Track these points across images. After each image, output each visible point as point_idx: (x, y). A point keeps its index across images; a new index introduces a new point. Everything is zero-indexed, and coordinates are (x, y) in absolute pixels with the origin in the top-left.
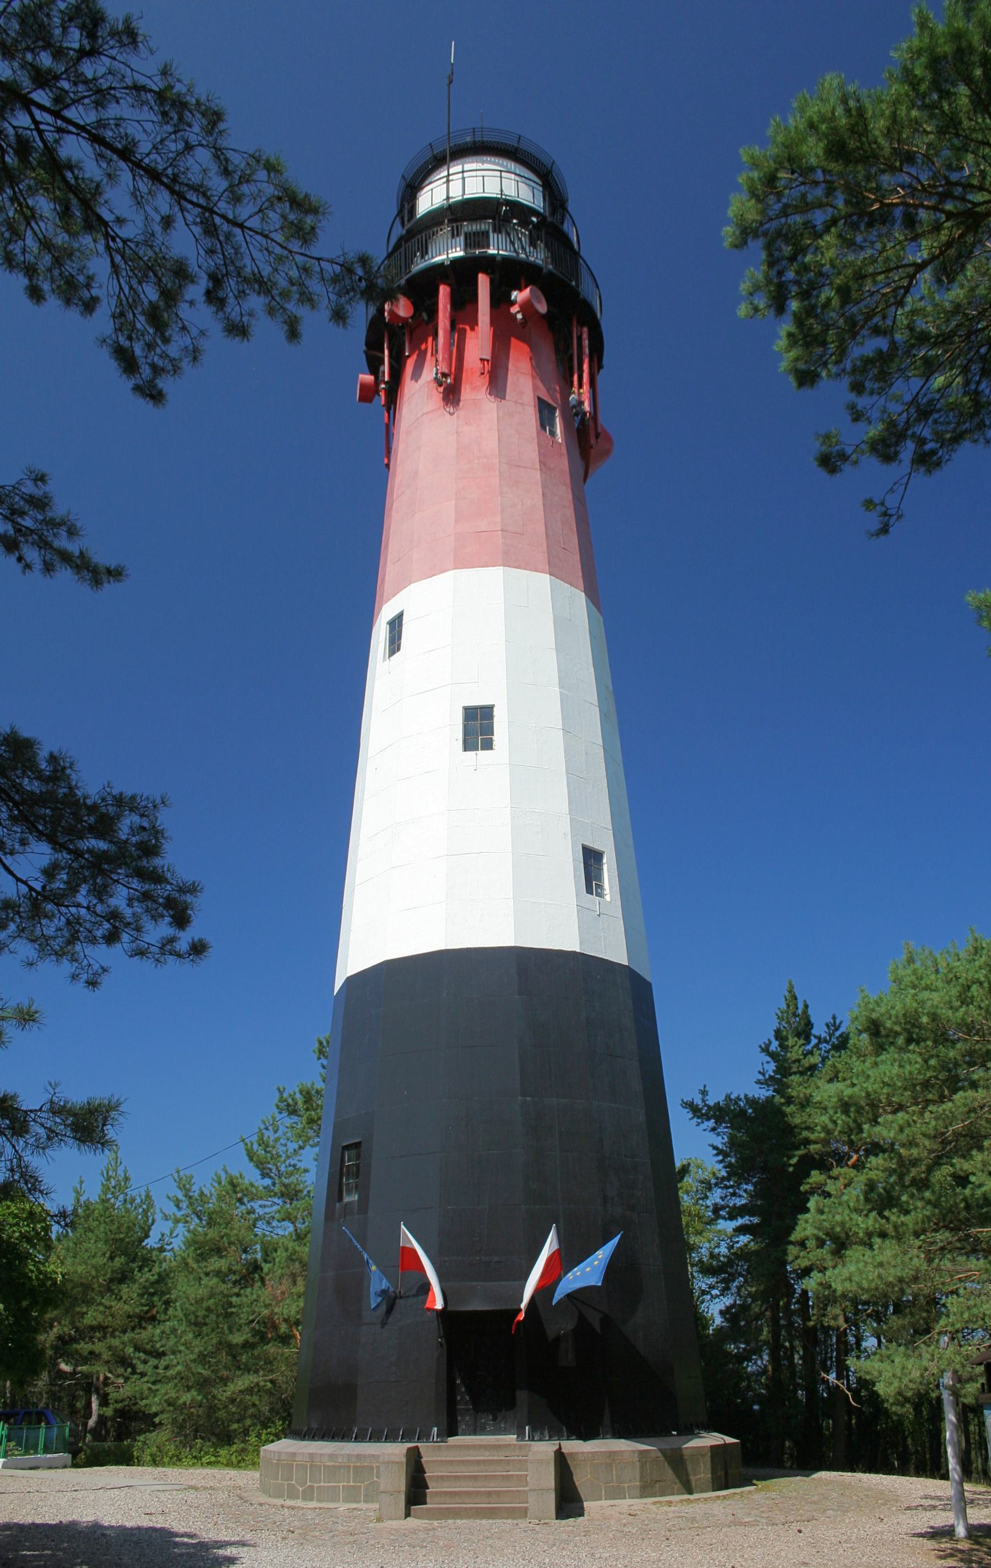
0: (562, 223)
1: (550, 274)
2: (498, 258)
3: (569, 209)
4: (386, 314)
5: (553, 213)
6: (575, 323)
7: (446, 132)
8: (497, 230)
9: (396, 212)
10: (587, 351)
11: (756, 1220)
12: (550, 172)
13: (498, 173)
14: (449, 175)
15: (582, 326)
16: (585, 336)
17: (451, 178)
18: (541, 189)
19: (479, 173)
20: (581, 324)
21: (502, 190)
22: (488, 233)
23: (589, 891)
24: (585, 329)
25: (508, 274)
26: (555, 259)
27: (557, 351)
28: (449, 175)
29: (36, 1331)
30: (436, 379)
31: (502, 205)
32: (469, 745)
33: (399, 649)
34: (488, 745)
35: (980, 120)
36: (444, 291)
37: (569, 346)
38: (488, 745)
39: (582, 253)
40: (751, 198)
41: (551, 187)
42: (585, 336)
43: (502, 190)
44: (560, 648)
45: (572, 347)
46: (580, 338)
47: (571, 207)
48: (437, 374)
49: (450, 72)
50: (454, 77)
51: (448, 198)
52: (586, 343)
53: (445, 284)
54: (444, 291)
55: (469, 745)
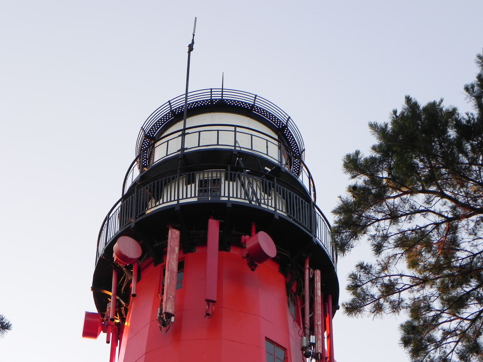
0: (298, 174)
1: (281, 218)
2: (229, 205)
4: (114, 255)
5: (290, 163)
6: (308, 266)
8: (230, 178)
11: (312, 346)
12: (286, 126)
13: (233, 128)
14: (185, 129)
15: (314, 269)
17: (187, 131)
18: (277, 143)
20: (314, 267)
21: (236, 142)
22: (219, 180)
24: (318, 272)
25: (241, 220)
26: (289, 208)
27: (289, 291)
28: (185, 129)
29: (380, 146)
30: (161, 318)
31: (236, 156)
36: (174, 236)
37: (301, 288)
39: (317, 204)
40: (366, 233)
41: (287, 140)
43: (236, 142)
45: (304, 290)
46: (312, 281)
47: (307, 159)
48: (161, 314)
50: (194, 46)
51: (183, 149)
53: (174, 228)
54: (174, 236)
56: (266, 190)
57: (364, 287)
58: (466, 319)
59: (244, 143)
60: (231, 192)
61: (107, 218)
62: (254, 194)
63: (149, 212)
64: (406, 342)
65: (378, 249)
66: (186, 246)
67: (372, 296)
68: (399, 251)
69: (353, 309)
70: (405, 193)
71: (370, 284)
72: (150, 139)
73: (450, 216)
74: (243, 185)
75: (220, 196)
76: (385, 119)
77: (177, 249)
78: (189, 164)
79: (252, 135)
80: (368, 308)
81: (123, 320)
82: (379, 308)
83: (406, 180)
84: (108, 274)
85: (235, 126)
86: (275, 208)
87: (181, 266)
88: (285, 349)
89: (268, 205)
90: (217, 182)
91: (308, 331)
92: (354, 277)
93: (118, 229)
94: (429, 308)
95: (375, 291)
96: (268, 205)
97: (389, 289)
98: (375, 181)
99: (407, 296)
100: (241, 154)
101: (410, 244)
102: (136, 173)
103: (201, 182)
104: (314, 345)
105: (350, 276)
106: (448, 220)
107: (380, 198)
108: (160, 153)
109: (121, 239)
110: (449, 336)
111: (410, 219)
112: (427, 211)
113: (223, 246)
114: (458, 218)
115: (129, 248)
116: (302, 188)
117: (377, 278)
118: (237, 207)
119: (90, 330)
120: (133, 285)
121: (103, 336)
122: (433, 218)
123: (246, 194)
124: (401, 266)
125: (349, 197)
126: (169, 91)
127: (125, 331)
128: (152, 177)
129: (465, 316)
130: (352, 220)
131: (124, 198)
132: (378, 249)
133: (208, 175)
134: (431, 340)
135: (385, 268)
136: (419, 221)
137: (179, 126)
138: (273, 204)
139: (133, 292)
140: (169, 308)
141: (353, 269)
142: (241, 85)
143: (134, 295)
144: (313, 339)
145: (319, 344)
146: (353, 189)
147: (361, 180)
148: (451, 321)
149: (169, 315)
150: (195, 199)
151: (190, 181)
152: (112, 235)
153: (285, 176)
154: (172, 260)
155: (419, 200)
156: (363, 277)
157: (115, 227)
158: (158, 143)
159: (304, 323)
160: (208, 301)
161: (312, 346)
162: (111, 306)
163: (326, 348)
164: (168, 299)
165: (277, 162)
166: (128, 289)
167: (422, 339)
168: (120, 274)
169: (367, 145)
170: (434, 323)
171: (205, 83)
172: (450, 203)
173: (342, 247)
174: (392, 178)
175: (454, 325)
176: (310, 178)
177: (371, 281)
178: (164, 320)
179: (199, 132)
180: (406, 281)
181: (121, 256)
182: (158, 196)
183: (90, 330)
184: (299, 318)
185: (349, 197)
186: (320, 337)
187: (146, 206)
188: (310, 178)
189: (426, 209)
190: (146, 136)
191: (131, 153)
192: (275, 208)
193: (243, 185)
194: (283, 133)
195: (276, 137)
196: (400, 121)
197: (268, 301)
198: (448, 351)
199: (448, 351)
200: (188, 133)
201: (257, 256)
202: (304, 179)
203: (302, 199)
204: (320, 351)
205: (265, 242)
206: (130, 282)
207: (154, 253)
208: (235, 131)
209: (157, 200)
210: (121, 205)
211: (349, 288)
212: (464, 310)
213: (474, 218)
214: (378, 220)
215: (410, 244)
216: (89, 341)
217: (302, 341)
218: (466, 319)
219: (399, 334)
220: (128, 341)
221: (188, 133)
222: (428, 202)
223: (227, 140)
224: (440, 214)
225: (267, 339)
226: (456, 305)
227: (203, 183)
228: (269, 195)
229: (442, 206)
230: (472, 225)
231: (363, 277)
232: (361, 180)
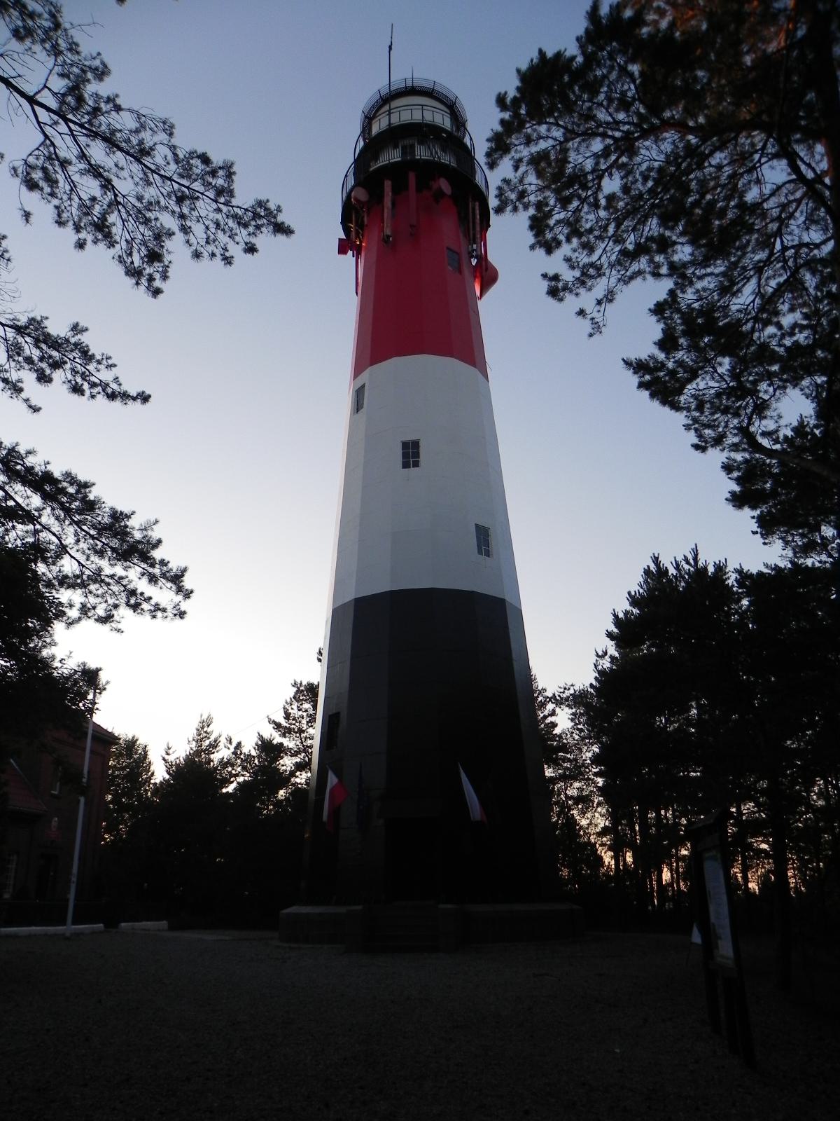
3: (468, 129)
5: (458, 129)
6: (471, 200)
7: (388, 83)
8: (421, 143)
9: (359, 133)
10: (478, 217)
11: (325, 818)
13: (421, 107)
14: (390, 110)
16: (477, 208)
17: (391, 111)
18: (449, 116)
19: (409, 107)
20: (474, 200)
23: (480, 552)
24: (477, 204)
25: (431, 170)
28: (390, 110)
30: (383, 239)
32: (416, 444)
33: (490, 226)
34: (416, 464)
35: (750, 325)
36: (388, 184)
38: (416, 464)
42: (477, 208)
44: (321, 674)
46: (474, 209)
47: (469, 126)
49: (390, 44)
50: (393, 47)
51: (390, 124)
52: (478, 212)
54: (388, 184)
55: (416, 444)
56: (444, 150)
57: (506, 195)
58: (571, 211)
59: (428, 117)
60: (421, 153)
61: (346, 176)
62: (436, 153)
63: (371, 169)
64: (531, 228)
65: (516, 168)
66: (396, 191)
67: (512, 200)
68: (530, 167)
69: (499, 210)
70: (534, 125)
71: (510, 192)
72: (368, 119)
73: (562, 139)
74: (429, 148)
75: (415, 155)
76: (524, 66)
77: (390, 194)
78: (396, 134)
79: (433, 111)
80: (509, 208)
81: (361, 242)
82: (515, 209)
83: (538, 115)
84: (351, 213)
85: (422, 105)
86: (450, 161)
87: (394, 204)
88: (457, 253)
89: (445, 160)
90: (412, 147)
91: (472, 242)
92: (499, 188)
93: (353, 182)
94: (547, 205)
95: (513, 196)
96: (445, 160)
97: (522, 195)
98: (516, 115)
99: (532, 198)
100: (427, 125)
101: (537, 161)
102: (361, 143)
103: (402, 148)
104: (475, 250)
105: (497, 188)
106: (561, 143)
107: (522, 125)
108: (375, 129)
109: (356, 188)
110: (600, 153)
111: (536, 144)
112: (548, 137)
113: (419, 190)
114: (567, 140)
115: (361, 194)
116: (467, 147)
117: (515, 187)
118: (426, 163)
119: (342, 249)
120: (365, 219)
121: (350, 253)
122: (551, 142)
123: (432, 154)
124: (532, 178)
125: (499, 128)
126: (377, 84)
127: (363, 249)
128: (372, 146)
129: (570, 209)
130: (500, 145)
131: (355, 161)
132: (516, 168)
133: (407, 142)
134: (548, 226)
135: (521, 181)
136: (543, 145)
137: (386, 108)
138: (447, 159)
139: (366, 222)
140: (388, 231)
141: (499, 183)
142: (425, 75)
143: (367, 226)
144: (475, 246)
145: (479, 250)
146: (502, 122)
147: (507, 115)
148: (560, 213)
149: (388, 237)
150: (400, 159)
151: (396, 147)
152: (350, 186)
153: (454, 140)
154: (388, 202)
155: (543, 129)
156: (506, 188)
157: (351, 181)
158: (374, 121)
159: (469, 236)
160: (412, 226)
161: (325, 818)
162: (353, 234)
163: (483, 252)
164: (387, 226)
165: (449, 129)
166: (363, 221)
167: (541, 226)
168: (357, 212)
169: (511, 86)
170: (549, 215)
171: (401, 77)
172: (562, 130)
173: (492, 165)
174: (528, 113)
175: (562, 216)
176: (471, 139)
177: (510, 190)
178: (385, 240)
179: (399, 111)
180: (533, 187)
181: (356, 199)
182: (376, 159)
183: (342, 249)
184: (467, 234)
185: (499, 128)
186: (479, 245)
187: (370, 167)
188: (471, 139)
189: (547, 136)
190: (366, 117)
191: (357, 130)
192: (450, 161)
193: (429, 148)
194: (452, 108)
195: (449, 112)
196: (533, 69)
197: (448, 226)
198: (557, 233)
199: (557, 233)
200: (393, 113)
201: (440, 194)
202: (467, 141)
203: (466, 155)
204: (479, 253)
205: (444, 185)
206: (364, 217)
207: (376, 197)
208: (422, 109)
209: (376, 161)
210: (354, 167)
211: (496, 196)
212: (569, 206)
213: (577, 140)
214: (516, 145)
215: (537, 161)
216: (343, 256)
217: (468, 248)
218: (571, 211)
219: (527, 223)
220: (366, 255)
221: (393, 113)
222: (549, 130)
223: (417, 117)
224: (555, 139)
225: (448, 248)
226: (564, 202)
227: (404, 148)
228: (446, 153)
229: (558, 133)
230: (576, 145)
231: (506, 188)
232: (507, 115)
